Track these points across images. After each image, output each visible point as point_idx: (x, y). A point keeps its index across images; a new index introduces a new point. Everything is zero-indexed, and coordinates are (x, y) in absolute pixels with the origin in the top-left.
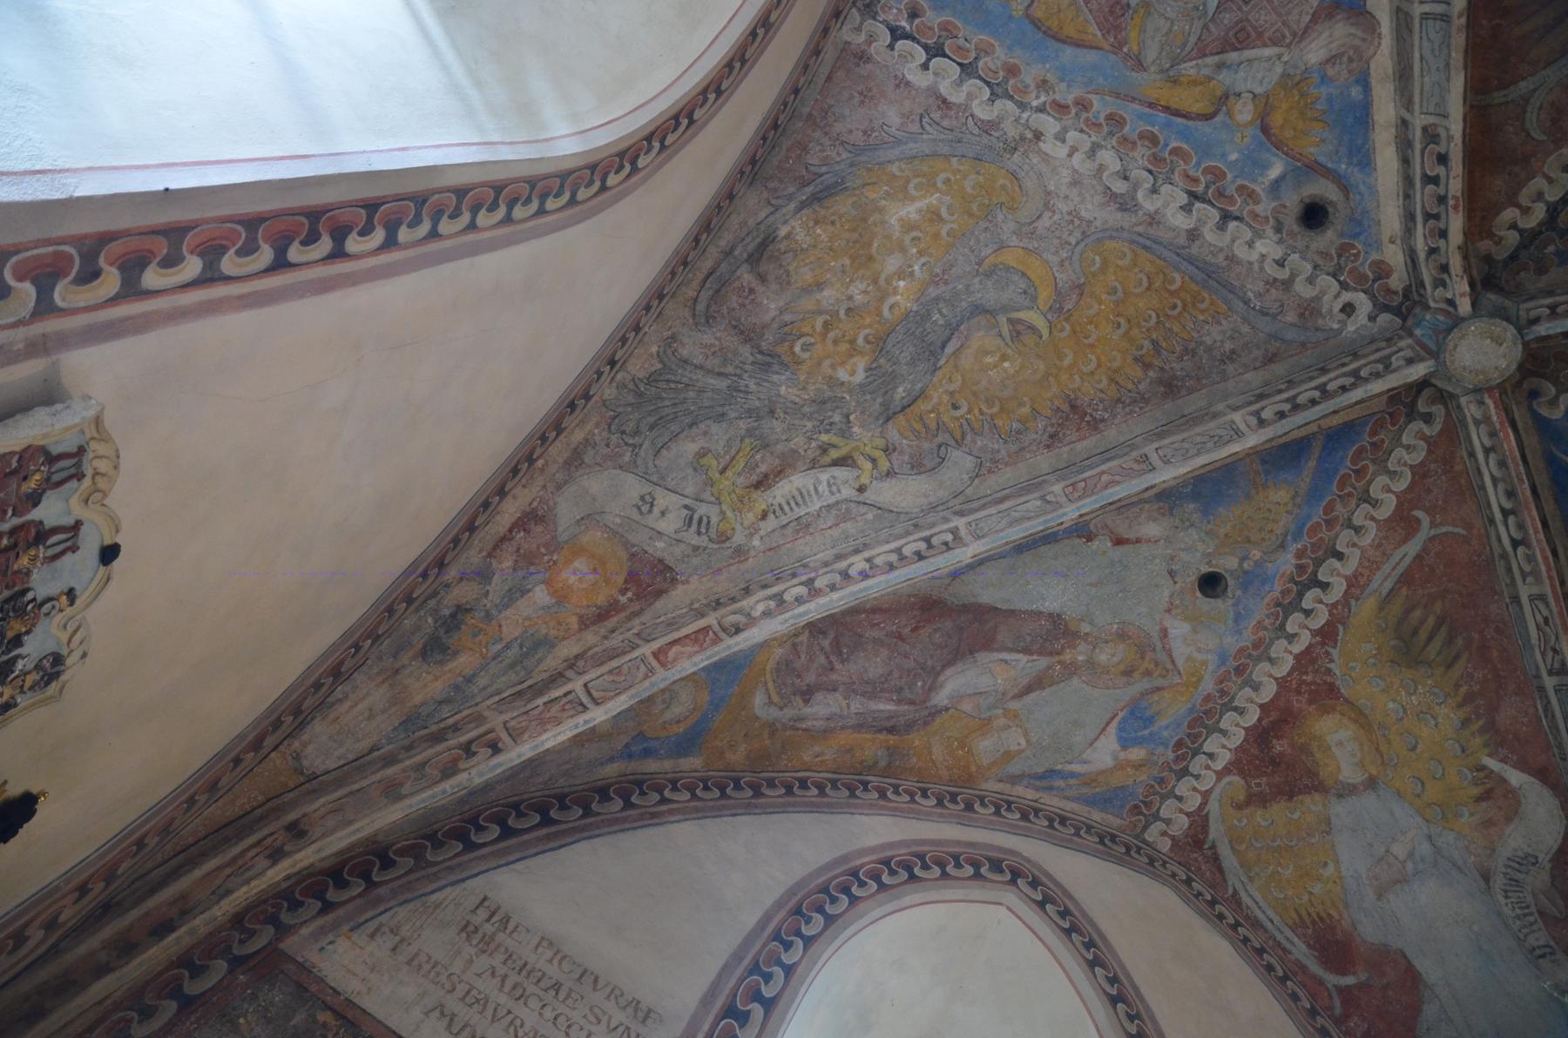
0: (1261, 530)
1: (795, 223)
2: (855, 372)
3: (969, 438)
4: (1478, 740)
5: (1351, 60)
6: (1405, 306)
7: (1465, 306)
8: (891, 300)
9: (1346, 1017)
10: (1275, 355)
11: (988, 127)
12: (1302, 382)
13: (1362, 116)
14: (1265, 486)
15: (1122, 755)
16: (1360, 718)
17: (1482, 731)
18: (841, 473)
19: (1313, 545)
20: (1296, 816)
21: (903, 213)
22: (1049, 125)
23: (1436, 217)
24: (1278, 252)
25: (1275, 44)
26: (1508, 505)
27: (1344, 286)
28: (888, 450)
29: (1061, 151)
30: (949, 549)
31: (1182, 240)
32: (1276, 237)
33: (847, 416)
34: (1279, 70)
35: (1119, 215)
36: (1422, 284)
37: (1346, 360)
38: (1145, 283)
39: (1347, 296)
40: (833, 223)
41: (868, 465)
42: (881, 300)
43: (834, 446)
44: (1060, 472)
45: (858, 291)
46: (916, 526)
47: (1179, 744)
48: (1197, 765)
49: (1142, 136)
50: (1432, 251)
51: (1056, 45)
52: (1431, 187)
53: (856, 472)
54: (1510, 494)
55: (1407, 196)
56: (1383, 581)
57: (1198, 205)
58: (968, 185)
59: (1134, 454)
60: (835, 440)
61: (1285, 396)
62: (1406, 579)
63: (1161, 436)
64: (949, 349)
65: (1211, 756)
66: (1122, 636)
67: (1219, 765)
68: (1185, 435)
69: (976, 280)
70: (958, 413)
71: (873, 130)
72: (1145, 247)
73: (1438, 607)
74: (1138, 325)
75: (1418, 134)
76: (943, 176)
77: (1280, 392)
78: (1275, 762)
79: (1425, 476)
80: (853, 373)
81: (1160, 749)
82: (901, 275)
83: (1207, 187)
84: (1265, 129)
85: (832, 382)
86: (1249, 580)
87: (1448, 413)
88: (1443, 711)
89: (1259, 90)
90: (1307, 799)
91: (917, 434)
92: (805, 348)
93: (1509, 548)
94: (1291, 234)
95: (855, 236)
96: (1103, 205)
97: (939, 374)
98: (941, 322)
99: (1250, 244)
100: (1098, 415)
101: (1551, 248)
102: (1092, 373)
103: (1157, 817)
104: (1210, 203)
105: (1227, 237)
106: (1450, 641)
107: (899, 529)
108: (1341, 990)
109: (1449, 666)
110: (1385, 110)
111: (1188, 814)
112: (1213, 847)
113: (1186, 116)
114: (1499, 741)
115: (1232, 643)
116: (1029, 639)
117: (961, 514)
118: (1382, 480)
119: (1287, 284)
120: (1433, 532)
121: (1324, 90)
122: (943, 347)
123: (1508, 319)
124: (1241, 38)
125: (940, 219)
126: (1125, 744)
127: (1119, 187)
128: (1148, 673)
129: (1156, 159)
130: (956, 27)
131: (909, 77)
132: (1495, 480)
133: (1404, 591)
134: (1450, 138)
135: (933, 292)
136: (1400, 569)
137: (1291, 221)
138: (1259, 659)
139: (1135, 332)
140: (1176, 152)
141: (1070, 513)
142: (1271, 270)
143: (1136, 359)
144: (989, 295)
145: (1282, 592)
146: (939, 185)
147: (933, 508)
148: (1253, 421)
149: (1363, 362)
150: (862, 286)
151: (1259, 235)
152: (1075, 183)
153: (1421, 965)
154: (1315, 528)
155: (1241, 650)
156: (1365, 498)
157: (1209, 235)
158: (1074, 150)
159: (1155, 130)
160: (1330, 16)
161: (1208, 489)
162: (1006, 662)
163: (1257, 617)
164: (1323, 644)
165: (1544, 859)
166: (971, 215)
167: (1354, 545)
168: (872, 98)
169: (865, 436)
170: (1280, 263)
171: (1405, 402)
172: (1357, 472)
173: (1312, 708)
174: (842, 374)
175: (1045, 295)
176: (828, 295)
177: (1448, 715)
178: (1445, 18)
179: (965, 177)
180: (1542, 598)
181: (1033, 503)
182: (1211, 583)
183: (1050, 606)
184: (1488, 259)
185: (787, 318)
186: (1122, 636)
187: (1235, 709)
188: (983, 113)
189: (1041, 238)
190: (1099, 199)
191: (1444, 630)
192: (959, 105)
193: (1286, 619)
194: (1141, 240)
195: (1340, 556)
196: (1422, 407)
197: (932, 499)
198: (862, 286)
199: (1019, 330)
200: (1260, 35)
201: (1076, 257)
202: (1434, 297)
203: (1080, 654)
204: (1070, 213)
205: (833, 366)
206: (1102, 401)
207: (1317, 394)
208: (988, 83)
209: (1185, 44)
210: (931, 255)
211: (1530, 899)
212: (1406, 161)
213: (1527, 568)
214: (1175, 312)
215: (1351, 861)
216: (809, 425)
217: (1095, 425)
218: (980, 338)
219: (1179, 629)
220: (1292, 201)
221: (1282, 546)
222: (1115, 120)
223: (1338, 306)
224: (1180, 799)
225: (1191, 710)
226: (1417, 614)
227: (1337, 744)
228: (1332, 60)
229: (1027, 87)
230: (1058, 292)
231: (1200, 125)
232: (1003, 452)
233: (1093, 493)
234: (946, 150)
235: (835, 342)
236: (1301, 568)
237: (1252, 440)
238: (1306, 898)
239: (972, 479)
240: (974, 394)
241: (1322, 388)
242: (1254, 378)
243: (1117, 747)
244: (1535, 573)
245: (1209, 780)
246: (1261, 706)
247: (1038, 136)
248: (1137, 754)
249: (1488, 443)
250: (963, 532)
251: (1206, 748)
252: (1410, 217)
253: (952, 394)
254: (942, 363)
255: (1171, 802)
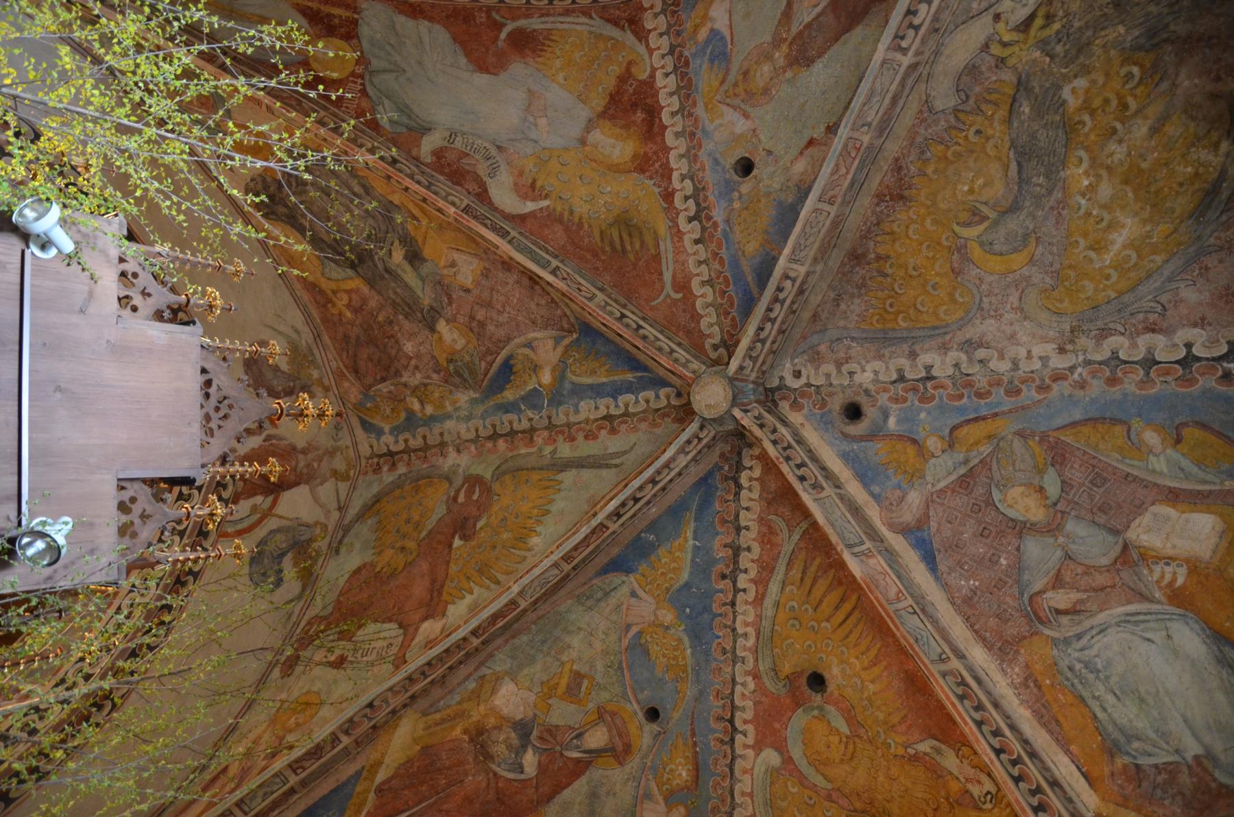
0: (745, 221)
1: (1216, 160)
2: (1071, 96)
3: (952, 120)
4: (559, 209)
5: (891, 504)
6: (770, 397)
7: (737, 413)
8: (1085, 165)
9: (489, 16)
10: (815, 321)
11: (1104, 333)
12: (786, 316)
13: (864, 478)
14: (762, 245)
15: (709, 25)
16: (616, 169)
17: (562, 215)
18: (1022, 13)
19: (713, 236)
20: (600, 89)
21: (1125, 232)
22: (1059, 362)
23: (785, 449)
24: (858, 378)
25: (941, 490)
26: (641, 331)
27: (809, 385)
28: (1001, 61)
29: (1036, 351)
30: (896, 36)
31: (917, 347)
32: (865, 386)
33: (1052, 57)
34: (929, 478)
35: (968, 336)
36: (769, 412)
37: (775, 346)
38: (919, 306)
39: (803, 380)
40: (1181, 185)
41: (1006, 38)
42: (1093, 159)
43: (1043, 27)
44: (871, 156)
45: (1117, 152)
46: (936, 30)
47: (687, 64)
48: (669, 62)
49: (989, 393)
50: (774, 431)
51: (1090, 415)
52: (799, 461)
53: (1012, 25)
54: (645, 338)
55: (810, 451)
56: (666, 246)
57: (924, 374)
58: (1090, 286)
59: (839, 200)
60: (1047, 32)
61: (788, 302)
62: (657, 258)
63: (836, 224)
64: (1014, 167)
65: (667, 75)
66: (766, 91)
67: (659, 74)
68: (821, 235)
69: (1031, 227)
70: (973, 130)
71: (1201, 274)
72: (935, 328)
73: (631, 256)
74: (903, 278)
75: (824, 484)
76: (1114, 278)
77: (793, 302)
78: (635, 106)
79: (692, 316)
80: (1074, 91)
81: (693, 50)
82: (1092, 188)
83: (925, 388)
84: (914, 441)
85: (1086, 70)
86: (728, 189)
87: (708, 357)
88: (586, 208)
89: (933, 460)
90: (603, 103)
91: (989, 91)
92: (1129, 76)
93: (624, 311)
94: (858, 394)
95: (1153, 189)
96: (984, 335)
97: (1007, 144)
98: (1034, 180)
99: (876, 373)
100: (883, 205)
101: (726, 468)
102: (907, 227)
103: (663, 11)
104: (917, 380)
105: (892, 368)
106: (612, 244)
107: (946, 16)
108: (504, 25)
109: (602, 232)
110: (854, 488)
111: (650, 31)
112: (623, 28)
113: (969, 421)
114: (551, 218)
115: (708, 146)
116: (814, 34)
117: (913, 67)
118: (710, 299)
119: (839, 365)
120: (665, 292)
121: (895, 481)
122: (1019, 164)
123: (714, 420)
124: (965, 482)
125: (1091, 248)
126: (714, 33)
127: (981, 353)
128: (736, 85)
129: (969, 385)
130: (1182, 386)
131: (1197, 331)
132: (657, 339)
133: (653, 251)
134: (805, 490)
135: (1058, 195)
136: (664, 260)
137: (862, 400)
138: (688, 151)
139: (902, 273)
140: (961, 397)
141: (843, 132)
142: (853, 366)
143: (889, 257)
144: (1013, 224)
145: (707, 197)
146: (1112, 271)
147: (937, 53)
148: (792, 274)
149: (765, 351)
150: (1117, 157)
151: (876, 381)
152: (1013, 336)
153: (486, 77)
154: (720, 246)
155: (700, 147)
156: (709, 282)
157: (904, 362)
158: (1029, 355)
159: (982, 402)
160: (919, 521)
161: (788, 215)
162: (815, 6)
163: (708, 172)
164: (666, 189)
165: (488, 181)
166: (1070, 267)
167: (695, 254)
168: (1221, 298)
169: (1026, 55)
170: (851, 374)
171: (729, 345)
172: (725, 292)
173: (642, 151)
174: (1081, 83)
175: (976, 252)
176: (1141, 129)
177: (581, 209)
178: (850, 546)
179: (1096, 290)
180: (590, 299)
181: (873, 116)
182: (746, 167)
183: (818, 66)
184: (750, 446)
185: (1165, 86)
186: (766, 91)
187: (676, 113)
188: (1115, 341)
189: (1008, 286)
190: (989, 337)
191: (619, 247)
192: (1138, 334)
193: (694, 185)
194: (943, 331)
195: (697, 242)
196: (722, 350)
197: (942, 59)
198: (1117, 157)
199: (976, 216)
200: (953, 491)
201: (975, 291)
202: (758, 410)
203: (779, 56)
204: (1001, 316)
205: (1094, 82)
206: (888, 215)
207: (773, 315)
208: (1126, 362)
209: (998, 462)
210: (1079, 218)
211: (477, 157)
212: (823, 468)
213: (608, 308)
214: (888, 302)
215: (556, 94)
216: (1077, 24)
217: (880, 197)
218: (998, 191)
219: (741, 126)
220: (870, 412)
221: (727, 221)
222: (1014, 392)
223: (804, 372)
224: (661, 35)
225: (697, 89)
226: (637, 246)
227: (617, 146)
228: (902, 499)
229: (1093, 377)
230: (970, 260)
231: (957, 421)
232: (922, 131)
233: (841, 154)
234: (1126, 298)
235: (1107, 101)
236: (709, 218)
237: (782, 262)
238: (558, 53)
239: (928, 96)
240: (972, 152)
241: (773, 321)
242: (815, 300)
243: (716, 26)
244: (603, 308)
245: (656, 60)
246: (666, 127)
247: (1062, 350)
248: (703, 34)
249: (675, 355)
250: (898, 56)
251: (673, 76)
252: (801, 441)
253: (988, 139)
254: (1011, 153)
255: (663, 28)
